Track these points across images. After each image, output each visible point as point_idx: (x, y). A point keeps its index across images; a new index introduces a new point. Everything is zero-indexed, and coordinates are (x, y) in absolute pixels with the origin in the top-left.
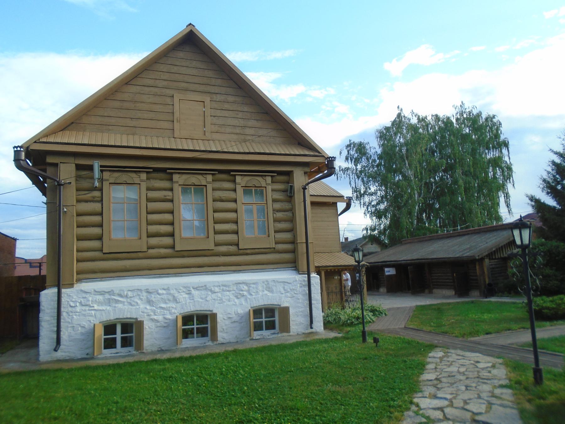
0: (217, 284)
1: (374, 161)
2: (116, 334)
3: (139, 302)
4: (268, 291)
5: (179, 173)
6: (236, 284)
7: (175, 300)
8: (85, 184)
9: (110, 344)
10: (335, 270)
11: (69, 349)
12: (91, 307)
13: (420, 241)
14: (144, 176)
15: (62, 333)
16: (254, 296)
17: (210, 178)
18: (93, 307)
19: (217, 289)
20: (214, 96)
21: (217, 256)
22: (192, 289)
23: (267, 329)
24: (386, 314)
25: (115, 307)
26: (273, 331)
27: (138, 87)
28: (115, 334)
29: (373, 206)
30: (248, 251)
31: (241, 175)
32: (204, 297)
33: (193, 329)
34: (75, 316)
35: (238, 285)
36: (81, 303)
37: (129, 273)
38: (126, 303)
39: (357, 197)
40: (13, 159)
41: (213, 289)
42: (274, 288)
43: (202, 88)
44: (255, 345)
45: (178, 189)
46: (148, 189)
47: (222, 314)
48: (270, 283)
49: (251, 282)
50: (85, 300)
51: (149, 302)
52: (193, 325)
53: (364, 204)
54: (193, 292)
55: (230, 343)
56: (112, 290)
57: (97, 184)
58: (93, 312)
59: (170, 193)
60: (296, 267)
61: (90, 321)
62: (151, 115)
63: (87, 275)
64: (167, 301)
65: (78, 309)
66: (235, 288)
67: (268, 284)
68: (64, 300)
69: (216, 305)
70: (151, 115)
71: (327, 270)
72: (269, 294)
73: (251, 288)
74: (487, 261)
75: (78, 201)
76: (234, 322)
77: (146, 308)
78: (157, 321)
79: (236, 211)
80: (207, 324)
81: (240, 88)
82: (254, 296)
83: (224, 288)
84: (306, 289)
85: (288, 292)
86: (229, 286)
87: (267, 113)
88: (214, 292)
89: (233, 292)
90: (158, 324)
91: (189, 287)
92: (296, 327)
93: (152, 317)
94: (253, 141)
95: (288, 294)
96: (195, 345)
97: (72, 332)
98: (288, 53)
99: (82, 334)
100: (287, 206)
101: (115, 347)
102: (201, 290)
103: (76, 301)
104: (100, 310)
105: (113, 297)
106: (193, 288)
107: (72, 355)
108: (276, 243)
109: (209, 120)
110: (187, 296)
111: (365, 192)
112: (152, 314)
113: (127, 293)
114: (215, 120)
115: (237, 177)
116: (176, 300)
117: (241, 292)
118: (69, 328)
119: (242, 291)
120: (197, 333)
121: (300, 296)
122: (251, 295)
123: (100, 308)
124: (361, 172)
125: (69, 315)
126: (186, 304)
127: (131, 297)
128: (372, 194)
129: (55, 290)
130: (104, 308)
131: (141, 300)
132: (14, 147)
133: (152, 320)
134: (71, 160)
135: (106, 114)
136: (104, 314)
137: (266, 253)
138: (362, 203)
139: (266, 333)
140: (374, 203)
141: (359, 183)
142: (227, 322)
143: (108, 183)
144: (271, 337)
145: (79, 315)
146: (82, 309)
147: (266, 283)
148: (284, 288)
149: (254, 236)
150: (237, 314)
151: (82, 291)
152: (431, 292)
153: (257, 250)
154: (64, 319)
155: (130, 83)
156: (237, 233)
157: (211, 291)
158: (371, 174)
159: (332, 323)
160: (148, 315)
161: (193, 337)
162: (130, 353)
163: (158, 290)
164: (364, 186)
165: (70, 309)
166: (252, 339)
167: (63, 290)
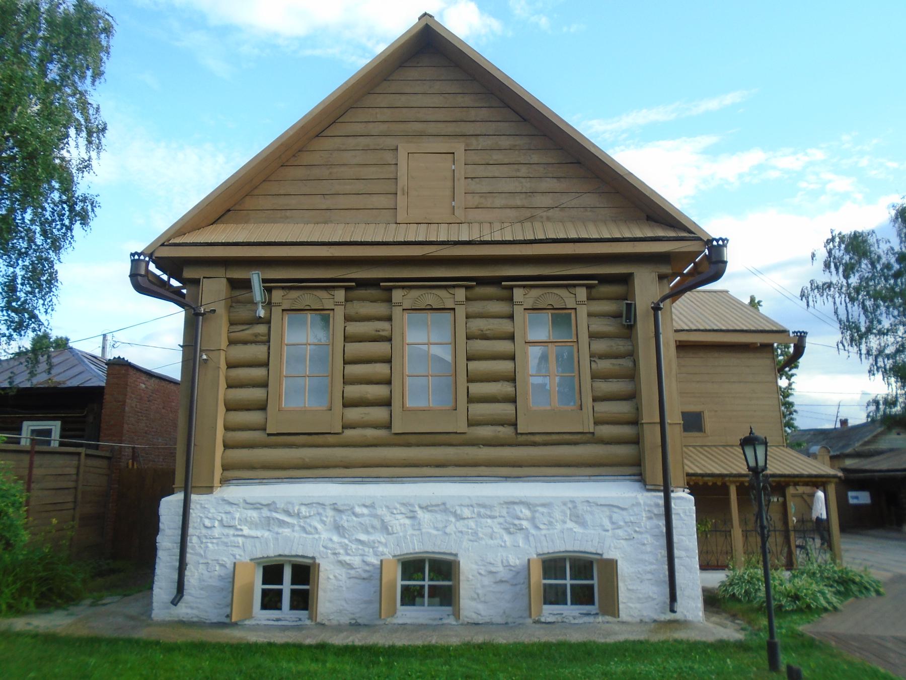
0: (467, 502)
1: (888, 266)
3: (319, 527)
4: (576, 522)
5: (403, 287)
6: (506, 503)
7: (385, 528)
8: (243, 313)
9: (271, 601)
10: (715, 484)
11: (198, 604)
12: (237, 529)
14: (340, 295)
15: (187, 573)
16: (544, 532)
17: (461, 294)
18: (241, 530)
19: (467, 512)
20: (473, 141)
21: (473, 445)
22: (417, 508)
23: (576, 601)
24: (878, 593)
25: (277, 533)
26: (586, 608)
27: (337, 140)
28: (281, 583)
29: (888, 357)
30: (537, 438)
31: (524, 287)
32: (440, 525)
33: (422, 587)
34: (210, 545)
35: (512, 506)
36: (221, 521)
38: (297, 528)
39: (852, 340)
40: (129, 274)
41: (459, 512)
42: (588, 518)
43: (451, 128)
44: (541, 636)
46: (348, 319)
47: (476, 563)
48: (580, 507)
49: (538, 502)
50: (229, 516)
51: (338, 528)
52: (424, 580)
53: (868, 353)
54: (420, 514)
55: (492, 624)
56: (274, 502)
57: (261, 313)
58: (240, 540)
59: (385, 325)
60: (640, 474)
61: (234, 556)
62: (359, 186)
63: (235, 472)
64: (371, 530)
65: (217, 532)
67: (575, 507)
68: (194, 514)
69: (465, 544)
70: (359, 186)
71: (742, 483)
72: (578, 529)
73: (537, 515)
75: (231, 342)
76: (501, 581)
77: (331, 540)
78: (349, 566)
79: (513, 358)
80: (402, 586)
81: (525, 120)
82: (544, 532)
83: (482, 511)
84: (662, 523)
85: (619, 527)
86: (491, 507)
87: (579, 163)
89: (501, 520)
90: (352, 572)
91: (412, 505)
92: (638, 606)
93: (342, 558)
94: (549, 219)
95: (620, 532)
97: (205, 572)
98: (729, 99)
99: (221, 578)
100: (620, 346)
101: (280, 609)
102: (436, 512)
103: (214, 519)
104: (253, 537)
106: (421, 507)
108: (596, 423)
109: (461, 185)
110: (408, 522)
111: (869, 330)
112: (342, 551)
113: (299, 510)
114: (474, 186)
115: (515, 291)
116: (387, 529)
117: (517, 522)
118: (201, 566)
119: (519, 519)
120: (430, 596)
121: (648, 539)
123: (253, 533)
124: (857, 290)
125: (202, 543)
126: (405, 537)
127: (306, 517)
128: (881, 333)
130: (258, 533)
131: (324, 523)
132: (133, 255)
133: (342, 563)
134: (220, 271)
135: (282, 192)
136: (258, 544)
137: (575, 443)
138: (864, 351)
139: (570, 611)
140: (890, 350)
141: (856, 311)
142: (486, 581)
143: (279, 309)
144: (581, 621)
145: (217, 544)
146: (225, 530)
147: (570, 505)
148: (610, 518)
149: (548, 408)
150: (508, 566)
151: (224, 500)
153: (554, 437)
154: (193, 548)
155: (324, 134)
156: (513, 400)
157: (455, 514)
158: (880, 292)
159: (739, 601)
160: (335, 554)
161: (423, 605)
162: (299, 623)
163: (352, 508)
164: (867, 317)
165: (204, 531)
166: (537, 622)
167: (194, 497)
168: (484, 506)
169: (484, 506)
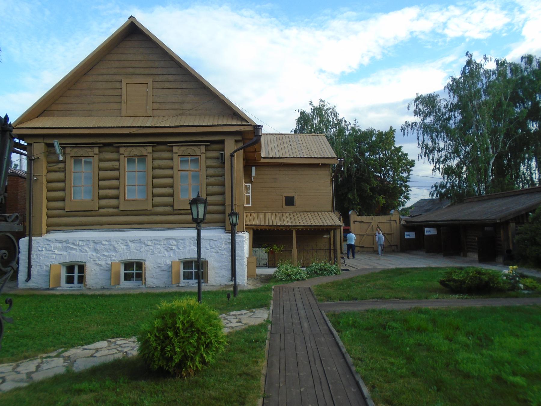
0: (149, 239)
2: (125, 273)
3: (88, 250)
5: (124, 146)
7: (115, 250)
11: (36, 282)
13: (479, 201)
17: (150, 149)
21: (155, 215)
22: (128, 242)
27: (94, 77)
30: (182, 212)
31: (178, 146)
38: (78, 250)
43: (147, 71)
45: (124, 161)
51: (96, 250)
53: (433, 160)
54: (130, 244)
56: (68, 240)
57: (61, 158)
58: (54, 256)
60: (225, 226)
63: (52, 228)
65: (44, 253)
66: (165, 243)
68: (34, 245)
69: (149, 256)
71: (298, 229)
74: (512, 225)
76: (164, 270)
83: (156, 242)
85: (213, 248)
86: (160, 241)
88: (147, 245)
89: (164, 246)
91: (127, 240)
92: (219, 279)
95: (213, 250)
96: (131, 287)
100: (218, 171)
101: (73, 283)
105: (68, 245)
107: (39, 286)
110: (125, 247)
112: (97, 259)
115: (174, 148)
117: (170, 246)
121: (225, 252)
122: (179, 249)
123: (59, 253)
130: (62, 253)
131: (89, 248)
135: (69, 102)
141: (427, 138)
142: (157, 270)
148: (210, 244)
152: (465, 255)
154: (34, 259)
155: (90, 73)
157: (145, 244)
165: (39, 252)
167: (33, 238)
168: (157, 240)
169: (157, 240)
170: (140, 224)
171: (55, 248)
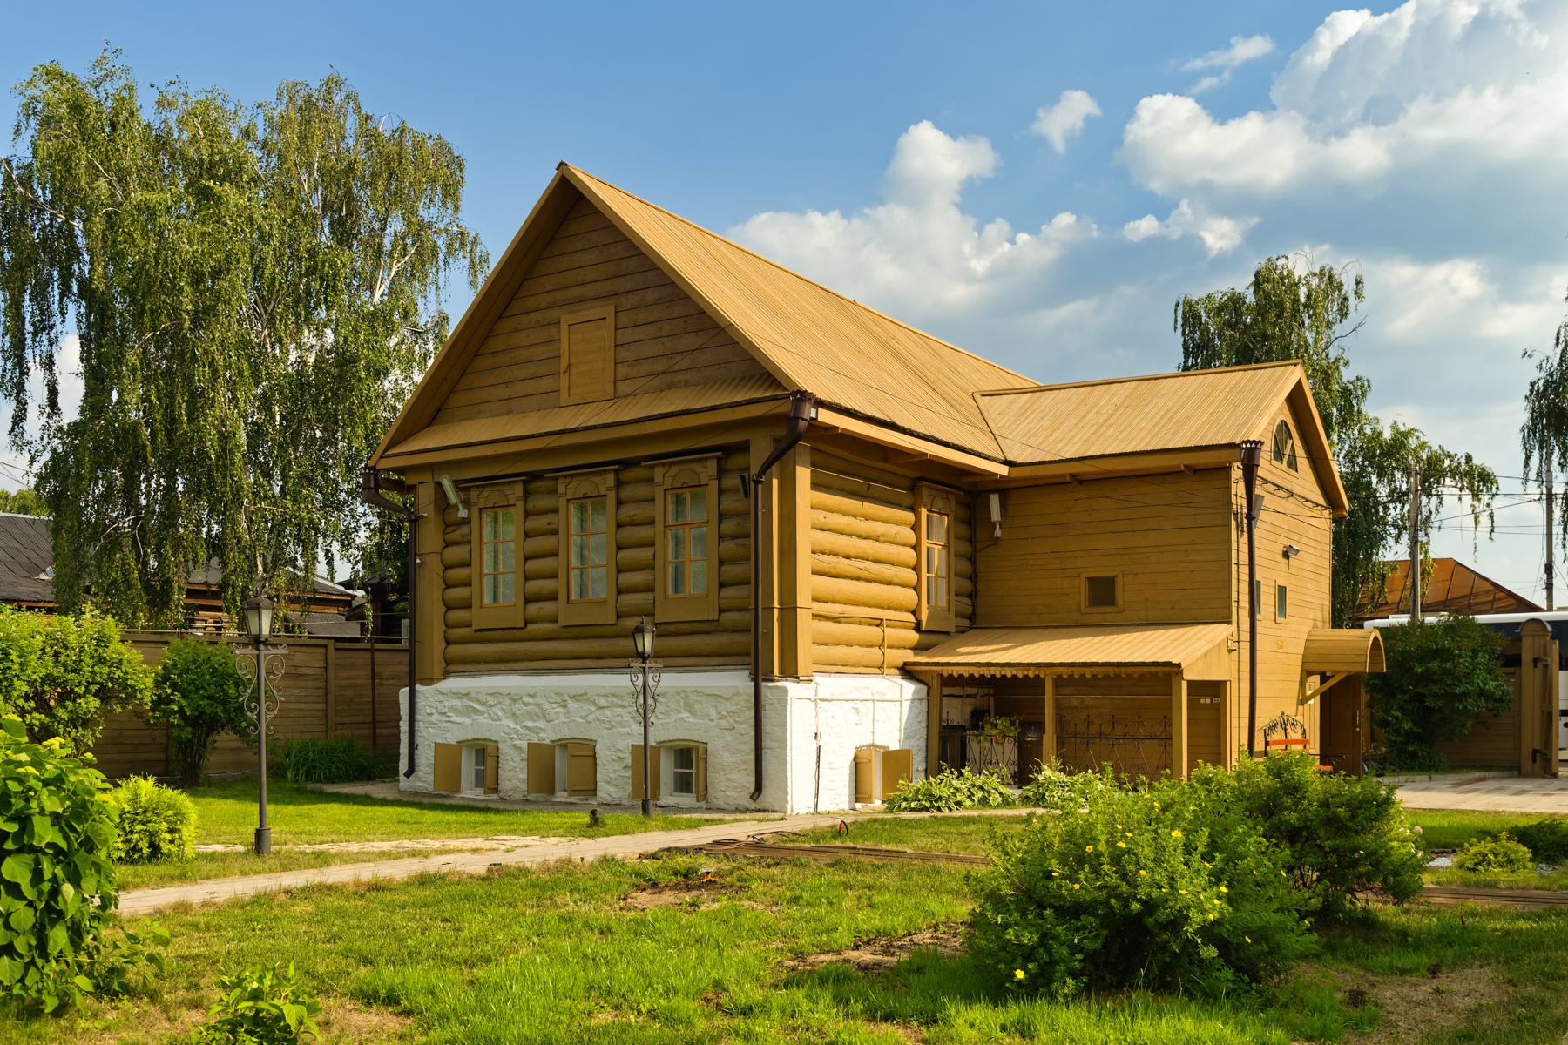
7: (544, 716)
10: (1071, 676)
37: (502, 666)
42: (697, 707)
63: (452, 666)
68: (420, 703)
71: (1060, 676)
85: (722, 718)
95: (723, 722)
106: (572, 697)
110: (560, 710)
129: (737, 682)
168: (614, 695)
169: (614, 695)
170: (598, 658)
171: (452, 709)
